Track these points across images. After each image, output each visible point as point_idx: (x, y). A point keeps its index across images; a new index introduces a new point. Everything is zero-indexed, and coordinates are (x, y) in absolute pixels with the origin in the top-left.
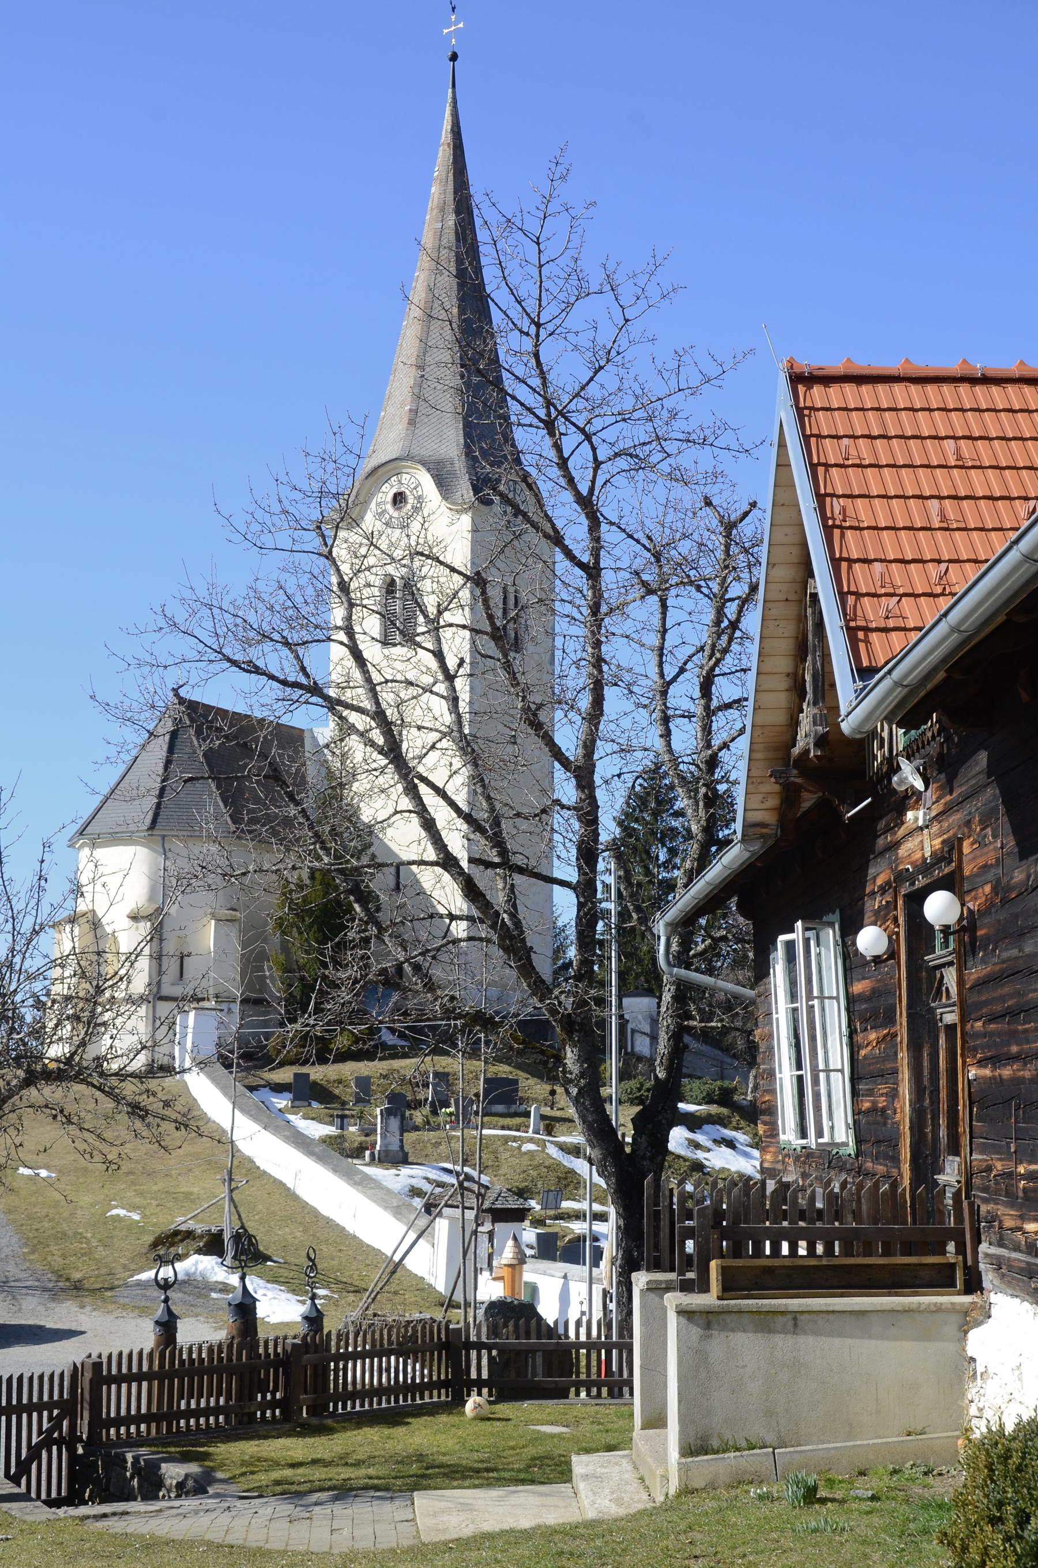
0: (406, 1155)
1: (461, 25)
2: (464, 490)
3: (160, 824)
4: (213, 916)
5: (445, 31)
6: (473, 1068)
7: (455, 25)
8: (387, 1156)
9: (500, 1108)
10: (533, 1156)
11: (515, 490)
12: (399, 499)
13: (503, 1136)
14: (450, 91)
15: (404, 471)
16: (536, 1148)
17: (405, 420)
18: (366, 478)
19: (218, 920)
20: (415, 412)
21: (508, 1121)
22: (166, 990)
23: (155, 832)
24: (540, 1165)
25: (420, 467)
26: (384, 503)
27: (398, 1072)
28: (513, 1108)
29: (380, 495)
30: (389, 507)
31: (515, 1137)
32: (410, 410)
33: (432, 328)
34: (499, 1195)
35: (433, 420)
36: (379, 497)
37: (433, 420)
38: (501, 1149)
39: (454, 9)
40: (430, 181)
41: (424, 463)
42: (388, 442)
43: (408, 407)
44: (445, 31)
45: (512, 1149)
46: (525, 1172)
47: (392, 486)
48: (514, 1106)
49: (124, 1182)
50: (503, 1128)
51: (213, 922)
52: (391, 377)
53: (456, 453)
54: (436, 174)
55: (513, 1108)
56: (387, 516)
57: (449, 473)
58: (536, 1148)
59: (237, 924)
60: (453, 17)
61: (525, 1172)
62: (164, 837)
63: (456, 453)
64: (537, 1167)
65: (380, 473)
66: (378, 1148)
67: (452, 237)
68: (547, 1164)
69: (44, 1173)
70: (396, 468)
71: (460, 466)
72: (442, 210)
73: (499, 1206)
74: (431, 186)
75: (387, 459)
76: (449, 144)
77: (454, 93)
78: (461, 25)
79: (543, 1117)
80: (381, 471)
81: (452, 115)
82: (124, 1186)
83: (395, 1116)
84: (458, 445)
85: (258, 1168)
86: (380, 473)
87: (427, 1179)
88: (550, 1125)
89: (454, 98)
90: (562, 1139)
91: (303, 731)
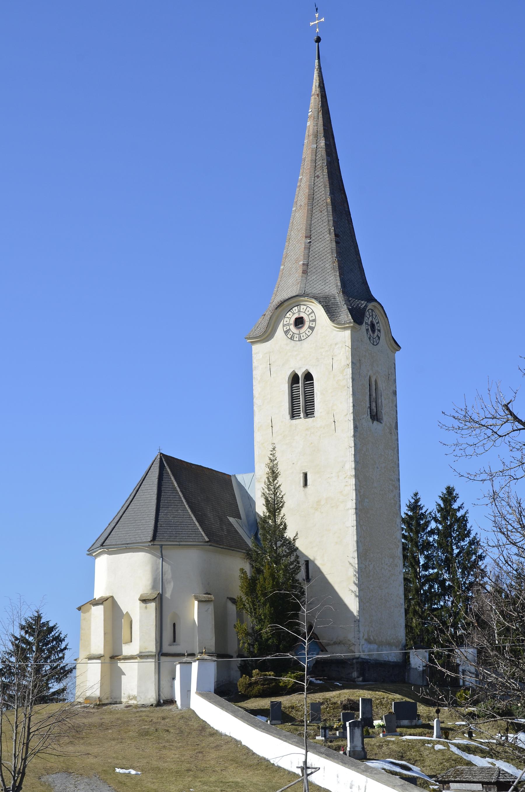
0: (365, 753)
1: (323, 20)
2: (345, 316)
3: (159, 539)
4: (196, 598)
5: (312, 24)
6: (377, 697)
7: (317, 21)
8: (354, 754)
9: (406, 722)
10: (443, 753)
11: (372, 316)
12: (299, 322)
13: (421, 740)
14: (317, 61)
15: (302, 303)
16: (444, 748)
17: (300, 271)
18: (276, 308)
19: (200, 601)
20: (306, 265)
21: (412, 731)
22: (166, 649)
23: (156, 543)
24: (449, 759)
25: (314, 301)
26: (289, 325)
27: (330, 700)
28: (414, 722)
29: (286, 319)
30: (292, 328)
31: (428, 740)
32: (303, 264)
33: (314, 211)
34: (500, 773)
35: (319, 271)
36: (286, 321)
37: (319, 271)
38: (422, 749)
39: (317, 9)
40: (306, 118)
41: (316, 299)
42: (289, 284)
43: (302, 262)
44: (312, 24)
45: (428, 749)
46: (441, 763)
47: (294, 314)
48: (414, 721)
49: (189, 777)
50: (410, 735)
51: (196, 603)
52: (287, 244)
53: (336, 291)
54: (309, 114)
55: (414, 722)
56: (291, 333)
57: (333, 304)
58: (444, 748)
59: (212, 603)
60: (317, 15)
61: (441, 763)
62: (161, 546)
63: (336, 291)
64: (448, 760)
65: (284, 306)
66: (348, 749)
67: (324, 153)
68: (453, 758)
69: (133, 772)
70: (296, 302)
71: (340, 299)
72: (316, 136)
73: (501, 780)
74: (307, 122)
75: (289, 296)
76: (318, 95)
77: (319, 62)
78: (323, 20)
79: (442, 729)
80: (286, 304)
81: (319, 76)
82: (190, 779)
83: (358, 727)
84: (337, 286)
85: (273, 764)
86: (284, 306)
87: (384, 769)
88: (445, 732)
89: (319, 65)
90: (454, 741)
91: (230, 476)
